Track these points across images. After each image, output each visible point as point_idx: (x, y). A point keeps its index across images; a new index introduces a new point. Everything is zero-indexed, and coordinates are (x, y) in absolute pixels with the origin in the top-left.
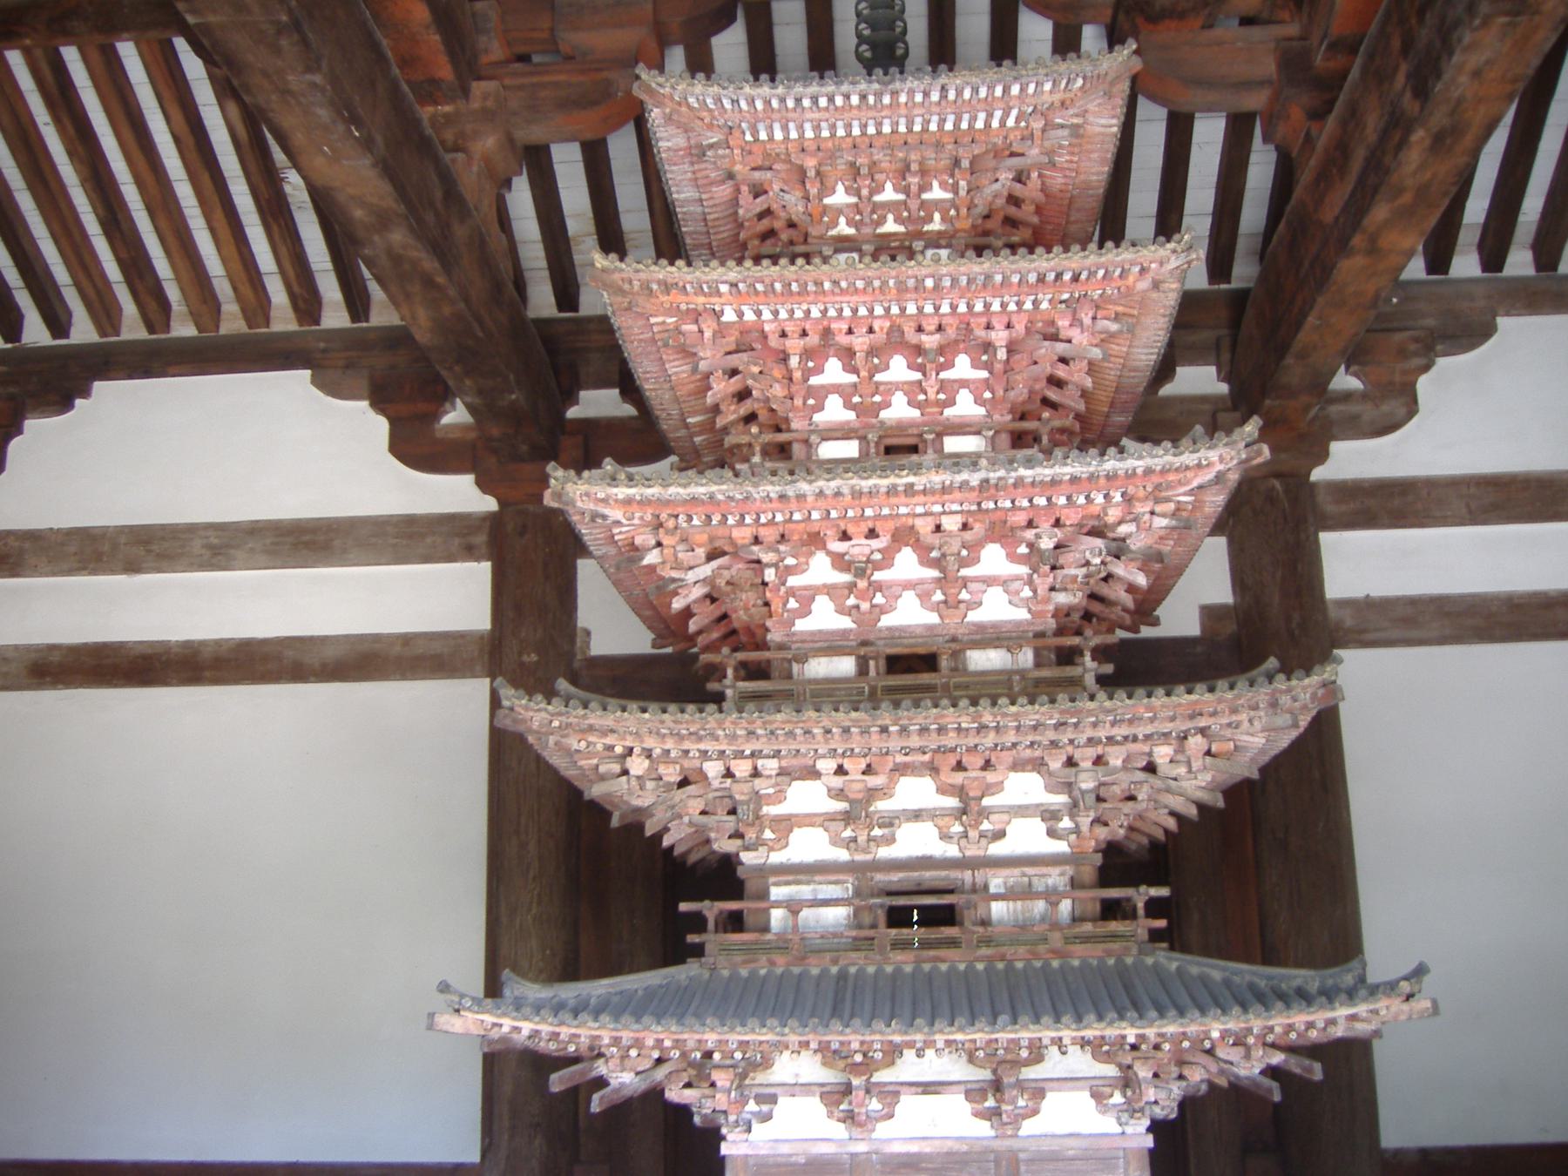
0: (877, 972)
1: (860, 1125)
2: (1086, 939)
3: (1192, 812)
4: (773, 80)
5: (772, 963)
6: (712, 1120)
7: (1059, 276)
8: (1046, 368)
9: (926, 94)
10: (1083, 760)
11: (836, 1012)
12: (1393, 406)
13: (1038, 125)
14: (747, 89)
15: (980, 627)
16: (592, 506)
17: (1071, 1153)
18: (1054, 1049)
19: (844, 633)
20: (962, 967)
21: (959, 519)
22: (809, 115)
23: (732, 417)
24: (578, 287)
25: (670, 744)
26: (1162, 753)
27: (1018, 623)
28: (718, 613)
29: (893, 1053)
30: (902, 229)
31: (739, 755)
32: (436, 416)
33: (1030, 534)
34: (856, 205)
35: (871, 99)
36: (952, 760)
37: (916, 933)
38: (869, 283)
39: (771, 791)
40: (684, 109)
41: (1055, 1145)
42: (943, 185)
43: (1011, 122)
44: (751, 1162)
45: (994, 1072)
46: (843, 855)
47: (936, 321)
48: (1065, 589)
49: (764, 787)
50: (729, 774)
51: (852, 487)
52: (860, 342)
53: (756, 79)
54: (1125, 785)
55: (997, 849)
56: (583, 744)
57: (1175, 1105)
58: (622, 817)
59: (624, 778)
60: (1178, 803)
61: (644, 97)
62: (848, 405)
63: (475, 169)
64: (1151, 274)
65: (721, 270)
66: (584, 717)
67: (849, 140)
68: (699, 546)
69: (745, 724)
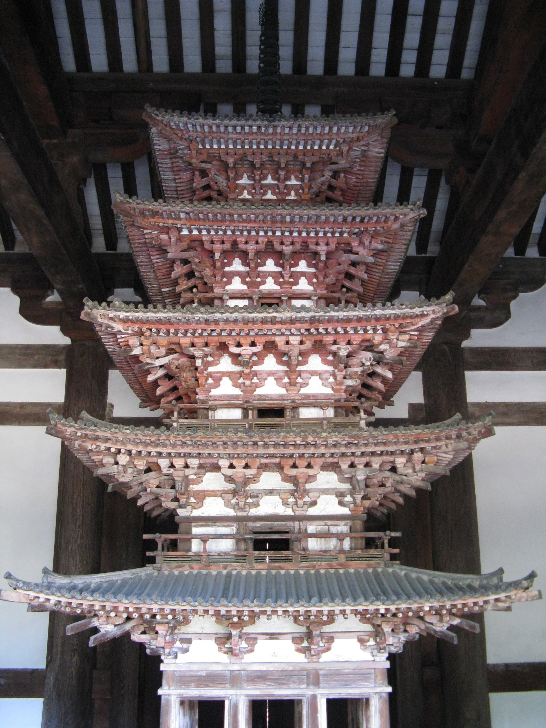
0: (247, 574)
1: (236, 655)
2: (359, 558)
3: (413, 493)
4: (214, 116)
5: (192, 568)
6: (156, 652)
7: (354, 218)
8: (345, 267)
9: (291, 128)
10: (359, 464)
11: (225, 595)
12: (498, 315)
13: (345, 148)
14: (201, 120)
15: (307, 397)
16: (106, 321)
17: (347, 671)
18: (341, 616)
19: (236, 397)
20: (292, 572)
21: (298, 338)
22: (231, 136)
23: (184, 287)
24: (117, 239)
25: (140, 448)
26: (400, 461)
27: (327, 395)
28: (172, 385)
29: (254, 617)
30: (275, 198)
31: (179, 455)
32: (44, 297)
33: (334, 348)
34: (253, 184)
35: (263, 129)
36: (291, 462)
37: (268, 555)
38: (257, 217)
39: (195, 477)
40: (168, 128)
41: (338, 667)
42: (297, 178)
43: (331, 147)
44: (177, 674)
45: (308, 628)
46: (231, 512)
47: (290, 239)
48: (352, 378)
49: (191, 474)
50: (172, 466)
51: (243, 317)
52: (251, 248)
53: (206, 115)
54: (380, 479)
55: (312, 511)
56: (94, 446)
57: (401, 645)
58: (114, 486)
59: (116, 466)
60: (405, 489)
61: (148, 120)
62: (244, 282)
63: (67, 171)
64: (400, 221)
65: (181, 205)
66: (95, 431)
67: (251, 150)
68: (163, 346)
69: (181, 438)
